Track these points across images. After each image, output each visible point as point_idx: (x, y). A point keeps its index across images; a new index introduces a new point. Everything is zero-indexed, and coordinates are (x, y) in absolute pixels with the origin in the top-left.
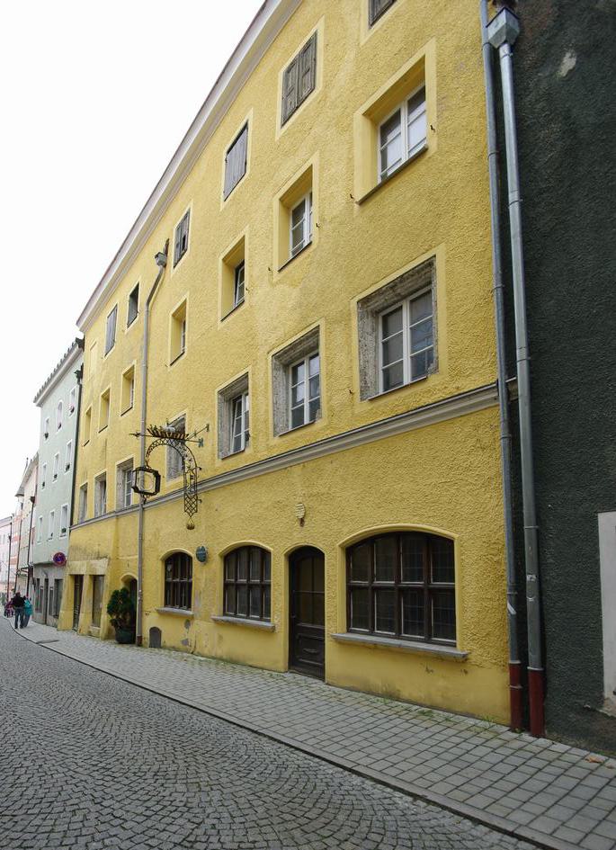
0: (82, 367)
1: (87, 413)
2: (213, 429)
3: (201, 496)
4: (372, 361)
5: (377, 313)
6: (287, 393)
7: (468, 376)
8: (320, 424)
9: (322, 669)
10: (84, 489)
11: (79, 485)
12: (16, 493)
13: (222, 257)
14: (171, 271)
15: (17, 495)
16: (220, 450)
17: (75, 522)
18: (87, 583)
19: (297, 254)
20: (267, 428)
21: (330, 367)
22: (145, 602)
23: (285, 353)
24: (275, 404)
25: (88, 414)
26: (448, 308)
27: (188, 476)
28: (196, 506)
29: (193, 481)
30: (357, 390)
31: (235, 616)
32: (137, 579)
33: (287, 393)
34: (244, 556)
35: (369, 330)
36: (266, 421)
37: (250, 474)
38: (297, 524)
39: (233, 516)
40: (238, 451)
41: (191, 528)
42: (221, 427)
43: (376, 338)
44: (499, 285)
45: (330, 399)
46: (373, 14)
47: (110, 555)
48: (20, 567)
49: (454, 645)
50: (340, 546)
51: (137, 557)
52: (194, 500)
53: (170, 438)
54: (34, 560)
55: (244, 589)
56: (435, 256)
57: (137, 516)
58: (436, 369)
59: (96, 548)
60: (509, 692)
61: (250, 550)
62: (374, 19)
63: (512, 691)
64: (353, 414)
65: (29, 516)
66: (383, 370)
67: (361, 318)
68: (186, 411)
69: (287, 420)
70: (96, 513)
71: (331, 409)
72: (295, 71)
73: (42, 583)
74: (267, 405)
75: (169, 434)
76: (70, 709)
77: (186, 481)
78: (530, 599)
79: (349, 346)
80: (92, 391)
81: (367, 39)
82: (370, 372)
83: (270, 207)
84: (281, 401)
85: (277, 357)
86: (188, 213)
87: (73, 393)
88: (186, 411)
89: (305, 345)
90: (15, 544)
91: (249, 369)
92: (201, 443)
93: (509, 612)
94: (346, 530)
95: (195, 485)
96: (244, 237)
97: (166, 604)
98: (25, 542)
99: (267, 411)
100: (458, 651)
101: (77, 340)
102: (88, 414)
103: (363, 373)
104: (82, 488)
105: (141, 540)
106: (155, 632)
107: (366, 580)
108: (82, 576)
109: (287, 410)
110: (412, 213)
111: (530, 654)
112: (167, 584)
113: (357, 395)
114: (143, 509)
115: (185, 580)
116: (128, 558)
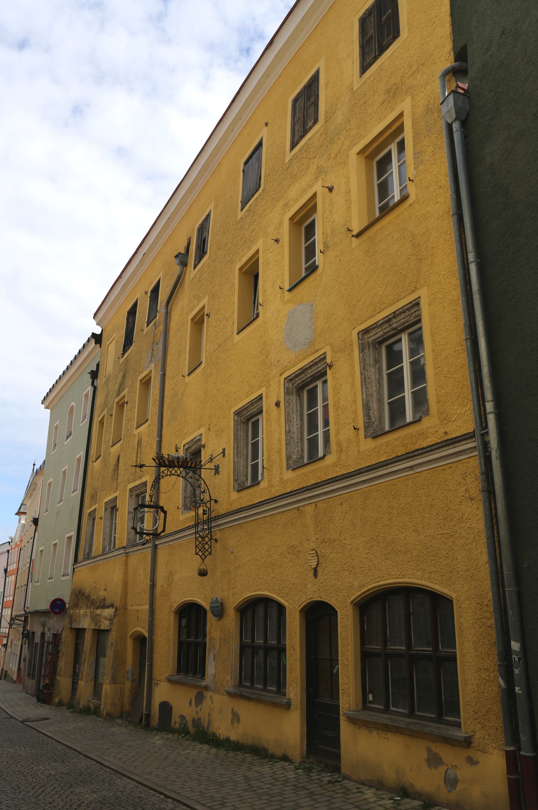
0: (98, 365)
1: (100, 422)
2: (229, 455)
3: (217, 535)
4: (375, 396)
5: (380, 343)
6: (302, 420)
7: (454, 421)
8: (330, 459)
9: (337, 757)
10: (93, 518)
11: (87, 511)
12: (16, 511)
13: (238, 266)
14: (191, 273)
15: (19, 513)
16: (236, 481)
17: (81, 556)
18: (88, 637)
19: (385, 210)
20: (281, 459)
21: (336, 399)
22: (155, 668)
23: (297, 376)
24: (288, 432)
25: (101, 423)
26: (433, 351)
27: (201, 511)
28: (210, 547)
29: (205, 516)
30: (361, 425)
31: (386, 710)
32: (146, 635)
33: (302, 420)
34: (260, 611)
35: (372, 362)
36: (279, 452)
37: (395, 472)
38: (311, 574)
39: (249, 561)
40: (313, 458)
41: (203, 573)
42: (237, 453)
43: (380, 370)
44: (468, 337)
45: (338, 432)
46: (292, 146)
47: (118, 603)
48: (14, 613)
49: (458, 725)
50: (352, 602)
51: (147, 607)
52: (207, 539)
53: (179, 467)
54: (32, 606)
55: (261, 653)
56: (420, 297)
57: (123, 558)
58: (331, 453)
59: (102, 593)
60: (506, 779)
61: (266, 601)
62: (364, 69)
63: (509, 779)
64: (359, 451)
65: (30, 545)
66: (389, 403)
67: (362, 349)
68: (202, 430)
69: (302, 451)
70: (104, 548)
71: (339, 444)
72: (301, 101)
73: (37, 639)
74: (280, 434)
75: (178, 462)
76: (39, 798)
77: (197, 514)
78: (516, 671)
79: (353, 377)
80: (107, 396)
81: (359, 85)
82: (374, 406)
83: (281, 224)
84: (295, 429)
85: (290, 380)
86: (209, 215)
87: (87, 396)
88: (202, 430)
89: (402, 319)
90: (11, 579)
91: (263, 391)
92: (217, 470)
93: (500, 686)
94: (356, 584)
95: (210, 520)
96: (258, 250)
97: (179, 671)
98: (23, 579)
99: (280, 440)
100: (461, 734)
101: (94, 335)
102: (101, 423)
103: (367, 407)
104: (90, 514)
105: (153, 586)
106: (166, 708)
107: (442, 648)
108: (84, 630)
109: (302, 439)
110: (399, 253)
111: (521, 735)
112: (181, 645)
113: (362, 432)
114: (156, 546)
115: (200, 640)
116: (138, 608)
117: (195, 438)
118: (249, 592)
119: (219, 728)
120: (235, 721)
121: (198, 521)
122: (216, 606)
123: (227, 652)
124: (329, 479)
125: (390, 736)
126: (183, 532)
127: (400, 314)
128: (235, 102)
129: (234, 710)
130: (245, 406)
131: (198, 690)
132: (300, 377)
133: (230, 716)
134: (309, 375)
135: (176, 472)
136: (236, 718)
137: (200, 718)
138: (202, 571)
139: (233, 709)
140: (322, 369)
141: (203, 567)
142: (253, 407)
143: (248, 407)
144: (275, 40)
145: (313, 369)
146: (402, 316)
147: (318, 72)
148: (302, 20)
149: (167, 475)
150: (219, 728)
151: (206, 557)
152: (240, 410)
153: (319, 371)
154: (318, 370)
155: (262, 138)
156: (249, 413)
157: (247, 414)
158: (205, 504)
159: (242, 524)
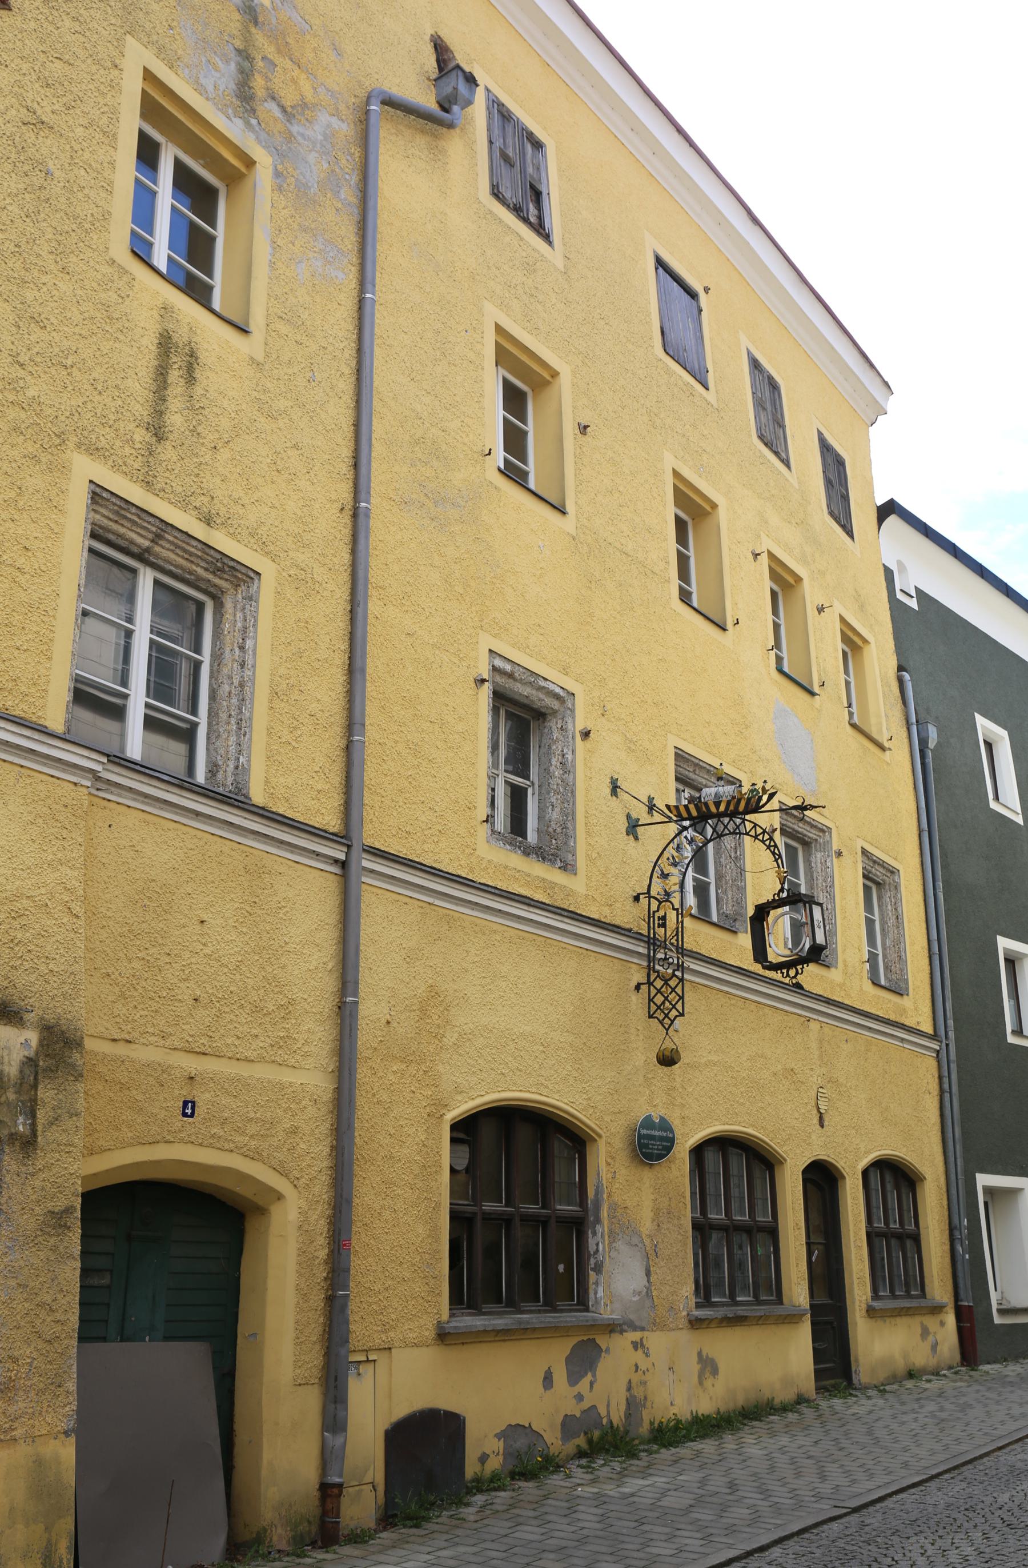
52: (673, 983)
58: (836, 967)
75: (717, 804)
117: (546, 679)
118: (717, 1123)
119: (672, 1404)
120: (707, 1375)
121: (677, 940)
122: (659, 1136)
123: (680, 1238)
124: (835, 1001)
125: (899, 1320)
126: (525, 907)
127: (884, 867)
128: (676, 134)
129: (704, 1354)
130: (701, 763)
131: (572, 1342)
132: (789, 819)
133: (696, 1368)
134: (796, 827)
135: (726, 827)
136: (708, 1366)
137: (594, 1407)
138: (667, 1053)
139: (700, 1354)
140: (809, 837)
141: (669, 1045)
142: (706, 777)
143: (702, 767)
144: (757, 228)
145: (805, 827)
146: (881, 870)
147: (749, 352)
148: (782, 287)
149: (763, 841)
150: (672, 1404)
151: (672, 1021)
152: (687, 756)
153: (805, 835)
154: (807, 833)
155: (749, 352)
156: (692, 775)
157: (687, 773)
158: (660, 903)
159: (699, 986)
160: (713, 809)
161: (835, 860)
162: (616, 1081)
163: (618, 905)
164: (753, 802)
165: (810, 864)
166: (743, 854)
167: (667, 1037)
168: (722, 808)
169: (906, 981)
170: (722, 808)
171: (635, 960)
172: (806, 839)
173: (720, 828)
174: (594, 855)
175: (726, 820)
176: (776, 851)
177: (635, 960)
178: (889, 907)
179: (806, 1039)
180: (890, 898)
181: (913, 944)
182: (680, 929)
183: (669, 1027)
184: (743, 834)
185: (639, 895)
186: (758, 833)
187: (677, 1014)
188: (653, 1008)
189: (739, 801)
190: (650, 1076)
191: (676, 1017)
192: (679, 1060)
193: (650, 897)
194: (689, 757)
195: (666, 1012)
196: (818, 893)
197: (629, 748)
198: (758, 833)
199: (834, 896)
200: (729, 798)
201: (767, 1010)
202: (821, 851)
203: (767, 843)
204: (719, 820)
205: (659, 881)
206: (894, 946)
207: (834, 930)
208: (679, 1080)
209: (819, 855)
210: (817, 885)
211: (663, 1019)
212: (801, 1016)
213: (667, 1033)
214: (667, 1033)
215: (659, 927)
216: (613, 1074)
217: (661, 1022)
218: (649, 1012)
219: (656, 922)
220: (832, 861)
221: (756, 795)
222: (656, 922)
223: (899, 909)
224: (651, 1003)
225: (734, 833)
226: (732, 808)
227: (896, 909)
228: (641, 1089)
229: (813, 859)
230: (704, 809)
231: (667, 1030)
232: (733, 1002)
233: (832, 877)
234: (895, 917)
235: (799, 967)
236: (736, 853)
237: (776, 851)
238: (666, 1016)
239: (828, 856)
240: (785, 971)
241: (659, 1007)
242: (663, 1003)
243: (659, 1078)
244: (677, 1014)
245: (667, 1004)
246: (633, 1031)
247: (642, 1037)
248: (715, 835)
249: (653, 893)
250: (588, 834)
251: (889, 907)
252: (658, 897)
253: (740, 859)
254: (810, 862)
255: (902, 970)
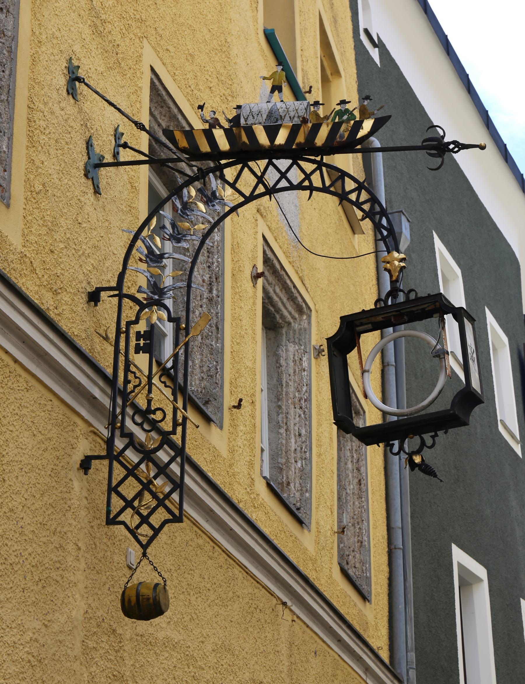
130: (180, 117)
135: (283, 175)
138: (146, 592)
140: (282, 317)
151: (157, 531)
160: (263, 139)
161: (313, 360)
162: (42, 641)
163: (66, 298)
164: (344, 130)
165: (277, 361)
166: (221, 295)
167: (145, 561)
168: (281, 138)
169: (369, 579)
170: (281, 138)
171: (84, 413)
172: (278, 316)
173: (272, 177)
174: (38, 187)
175: (283, 164)
176: (384, 222)
177: (84, 413)
178: (350, 465)
179: (276, 637)
180: (351, 450)
181: (375, 528)
182: (182, 358)
183: (151, 540)
184: (318, 189)
185: (99, 290)
186: (348, 189)
187: (169, 517)
188: (117, 503)
189: (316, 128)
190: (91, 644)
191: (166, 522)
192: (167, 608)
193: (121, 296)
194: (166, 98)
195: (145, 513)
196: (288, 406)
197: (96, 26)
198: (348, 189)
199: (310, 417)
200: (297, 121)
201: (237, 570)
202: (294, 342)
203: (366, 207)
204: (270, 163)
205: (143, 266)
206: (353, 525)
207: (308, 468)
208: (129, 662)
209: (292, 348)
210: (287, 394)
211: (138, 527)
212: (272, 594)
213: (144, 555)
214: (144, 555)
215: (137, 352)
216: (37, 624)
217: (133, 532)
218: (108, 512)
219: (133, 342)
220: (309, 360)
221: (348, 121)
222: (133, 342)
223: (363, 469)
224: (114, 495)
225: (300, 187)
226: (301, 138)
227: (358, 470)
228: (76, 666)
229: (282, 353)
230: (245, 138)
231: (144, 547)
232: (201, 542)
233: (309, 385)
234: (356, 481)
235: (427, 437)
236: (211, 291)
237: (384, 222)
238: (145, 520)
239: (305, 352)
240: (396, 443)
241: (129, 504)
242: (139, 495)
243: (102, 652)
244: (169, 517)
245: (147, 496)
246: (71, 547)
247: (83, 566)
248: (261, 189)
249: (129, 288)
250: (32, 142)
251: (350, 465)
252: (140, 296)
253: (217, 303)
254: (277, 358)
255: (363, 563)
